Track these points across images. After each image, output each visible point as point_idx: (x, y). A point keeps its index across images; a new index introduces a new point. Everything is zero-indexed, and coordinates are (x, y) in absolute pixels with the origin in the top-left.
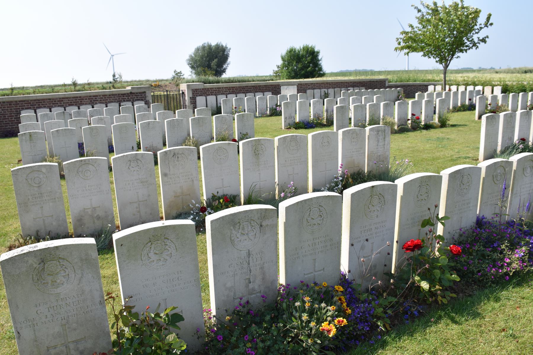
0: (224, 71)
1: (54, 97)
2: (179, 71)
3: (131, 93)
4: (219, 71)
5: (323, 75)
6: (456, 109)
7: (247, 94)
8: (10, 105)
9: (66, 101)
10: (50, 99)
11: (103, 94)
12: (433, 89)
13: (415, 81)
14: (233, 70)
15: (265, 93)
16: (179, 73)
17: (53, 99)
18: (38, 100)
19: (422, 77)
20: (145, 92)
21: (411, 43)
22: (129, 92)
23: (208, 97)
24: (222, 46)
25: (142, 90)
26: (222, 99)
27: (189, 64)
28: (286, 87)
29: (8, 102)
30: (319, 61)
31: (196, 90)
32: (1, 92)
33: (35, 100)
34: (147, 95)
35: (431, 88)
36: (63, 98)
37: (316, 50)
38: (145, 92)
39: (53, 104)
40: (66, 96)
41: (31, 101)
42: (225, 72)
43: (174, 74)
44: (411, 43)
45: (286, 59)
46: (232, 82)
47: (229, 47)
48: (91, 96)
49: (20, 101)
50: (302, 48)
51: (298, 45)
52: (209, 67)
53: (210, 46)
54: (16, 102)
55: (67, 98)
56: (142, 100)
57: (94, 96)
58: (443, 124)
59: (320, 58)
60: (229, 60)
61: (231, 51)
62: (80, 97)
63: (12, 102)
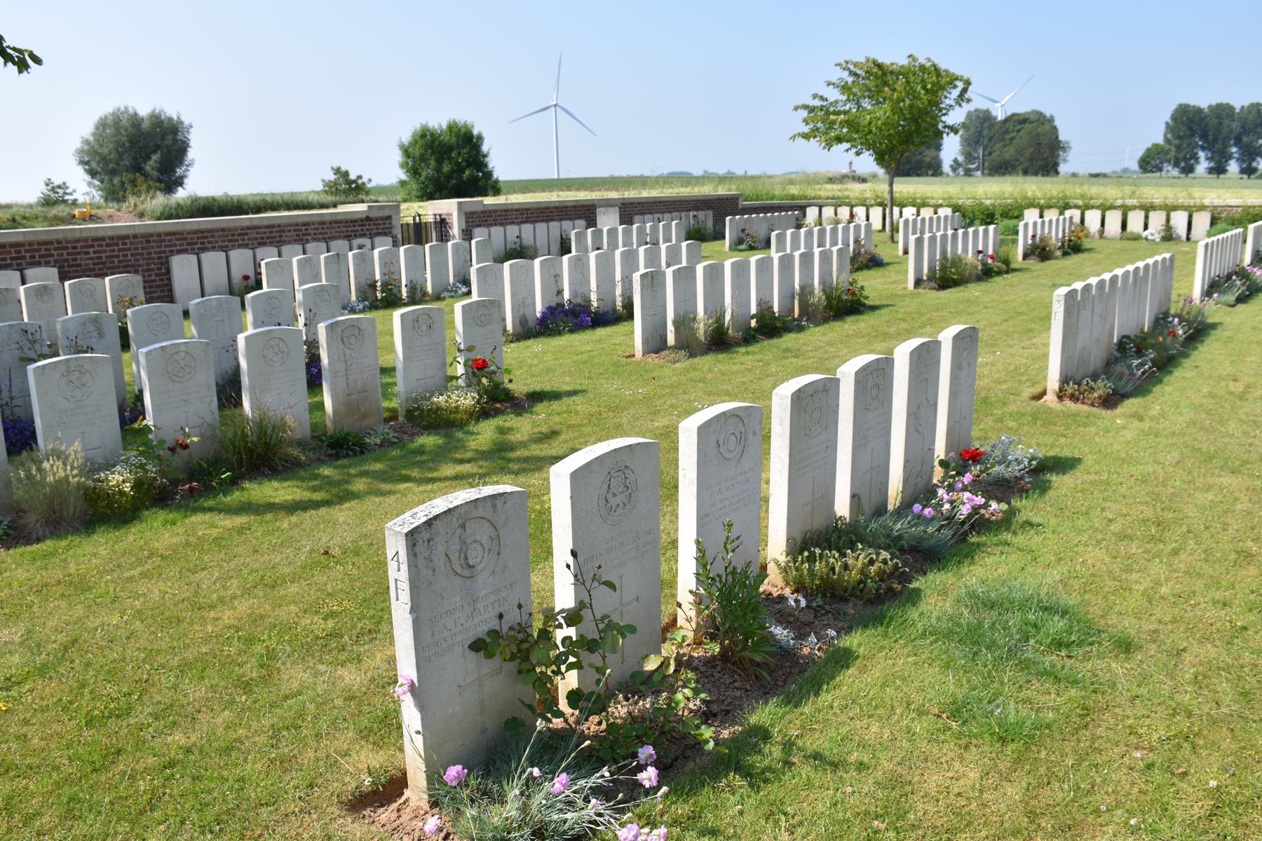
0: (179, 182)
1: (232, 225)
2: (57, 182)
3: (368, 218)
4: (171, 182)
5: (495, 188)
6: (529, 330)
7: (30, 272)
8: (148, 242)
9: (253, 234)
10: (223, 230)
11: (319, 219)
12: (832, 214)
13: (772, 199)
14: (204, 178)
15: (285, 249)
16: (59, 187)
17: (230, 230)
18: (202, 232)
19: (794, 190)
20: (389, 217)
21: (825, 124)
22: (364, 216)
23: (204, 256)
24: (171, 119)
25: (386, 213)
26: (268, 257)
27: (82, 163)
28: (603, 209)
29: (143, 236)
30: (485, 156)
31: (472, 213)
32: (5, 215)
33: (195, 232)
34: (394, 223)
35: (812, 213)
36: (248, 228)
37: (475, 132)
38: (389, 217)
39: (230, 241)
40: (255, 223)
41: (189, 233)
42: (181, 184)
43: (44, 189)
44: (825, 124)
45: (417, 152)
46: (274, 207)
47: (186, 121)
48: (297, 225)
49: (166, 234)
50: (444, 127)
51: (438, 121)
52: (137, 168)
53: (136, 121)
54: (159, 235)
55: (255, 228)
56: (386, 234)
57: (304, 224)
58: (498, 400)
59: (485, 148)
60: (191, 154)
61: (192, 130)
62: (279, 226)
63: (151, 235)
